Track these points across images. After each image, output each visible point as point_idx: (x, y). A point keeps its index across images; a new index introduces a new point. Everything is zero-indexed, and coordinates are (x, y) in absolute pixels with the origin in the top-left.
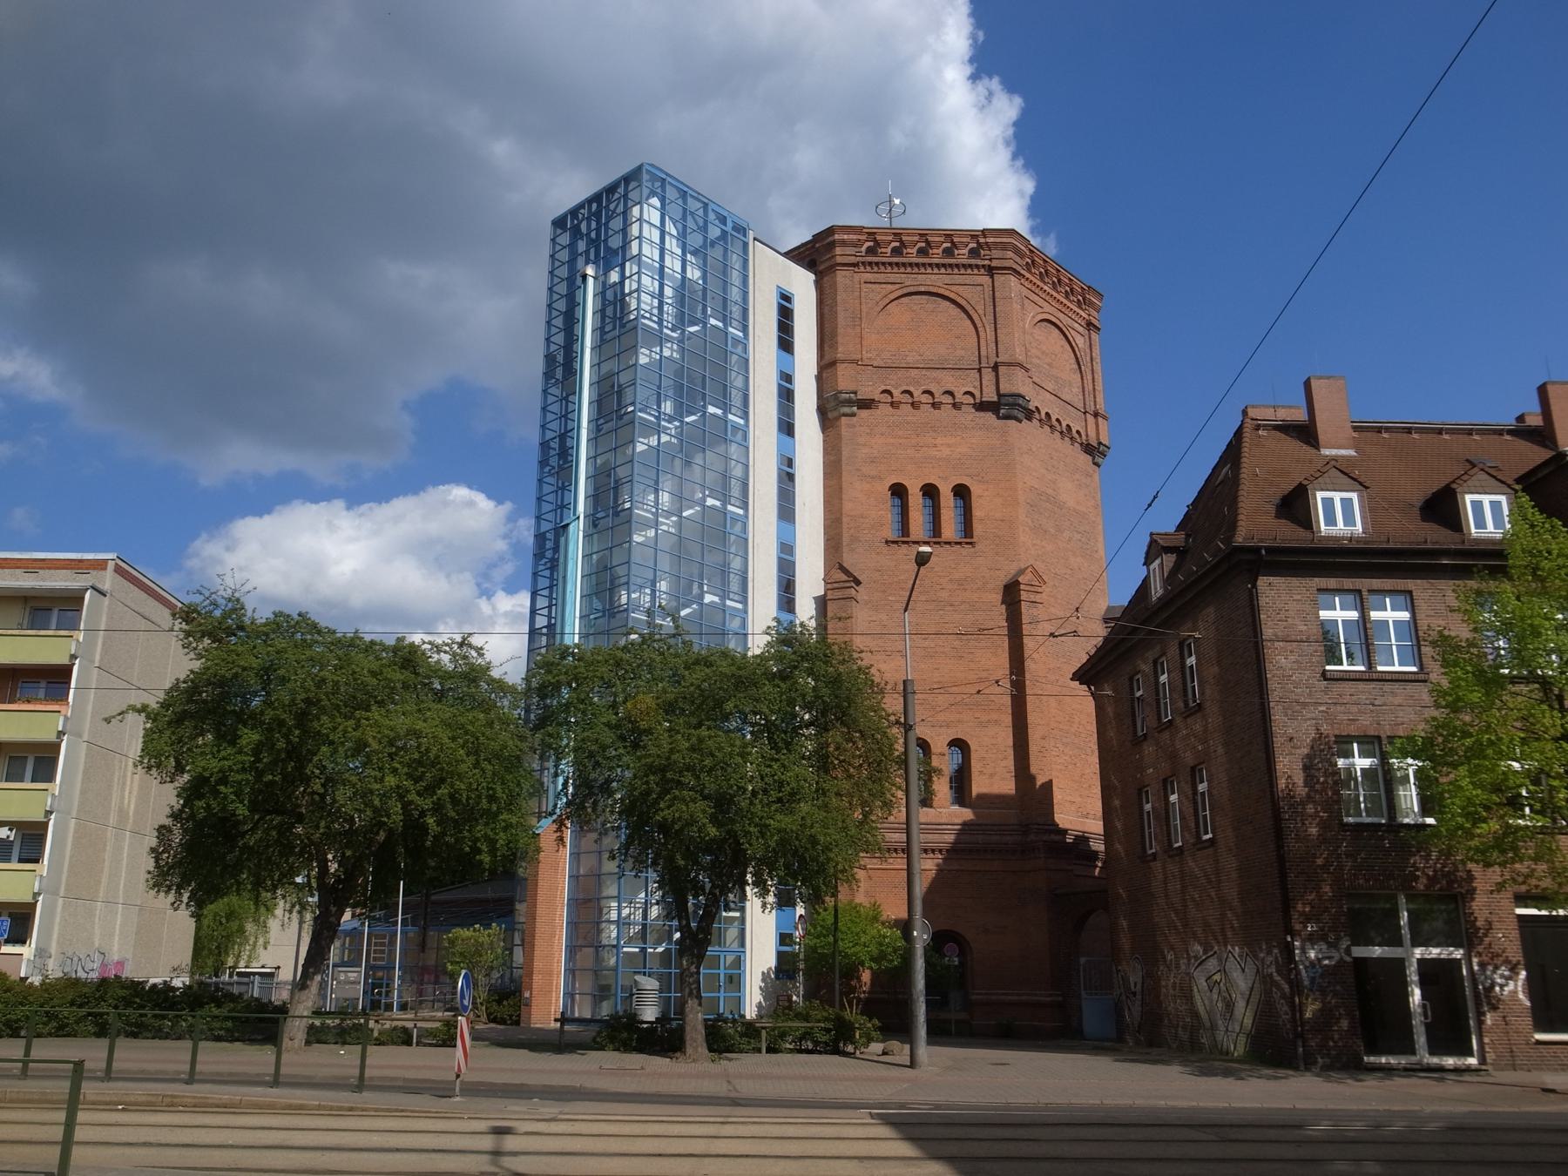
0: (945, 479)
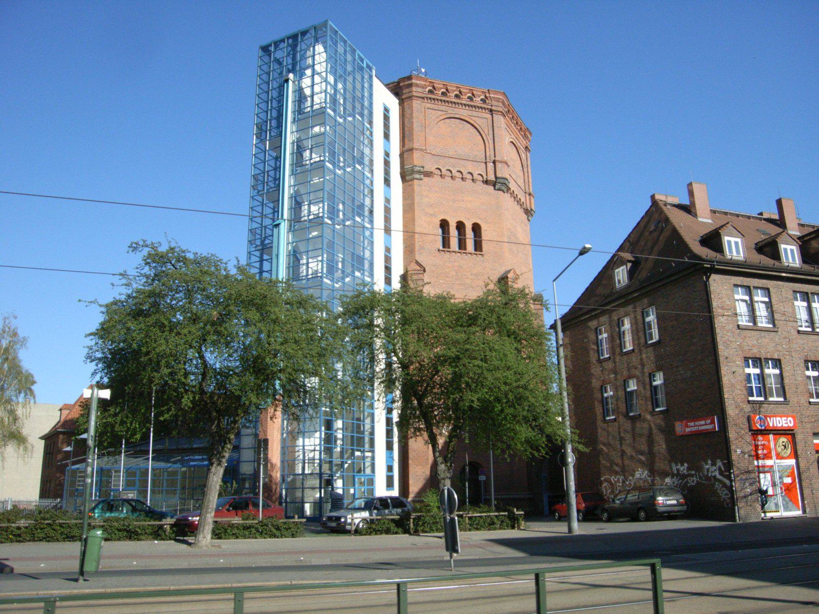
0: (469, 219)
